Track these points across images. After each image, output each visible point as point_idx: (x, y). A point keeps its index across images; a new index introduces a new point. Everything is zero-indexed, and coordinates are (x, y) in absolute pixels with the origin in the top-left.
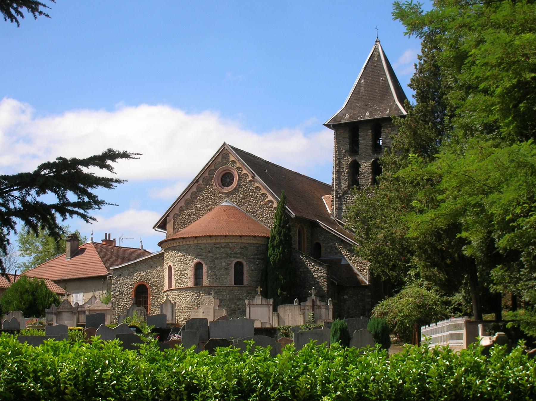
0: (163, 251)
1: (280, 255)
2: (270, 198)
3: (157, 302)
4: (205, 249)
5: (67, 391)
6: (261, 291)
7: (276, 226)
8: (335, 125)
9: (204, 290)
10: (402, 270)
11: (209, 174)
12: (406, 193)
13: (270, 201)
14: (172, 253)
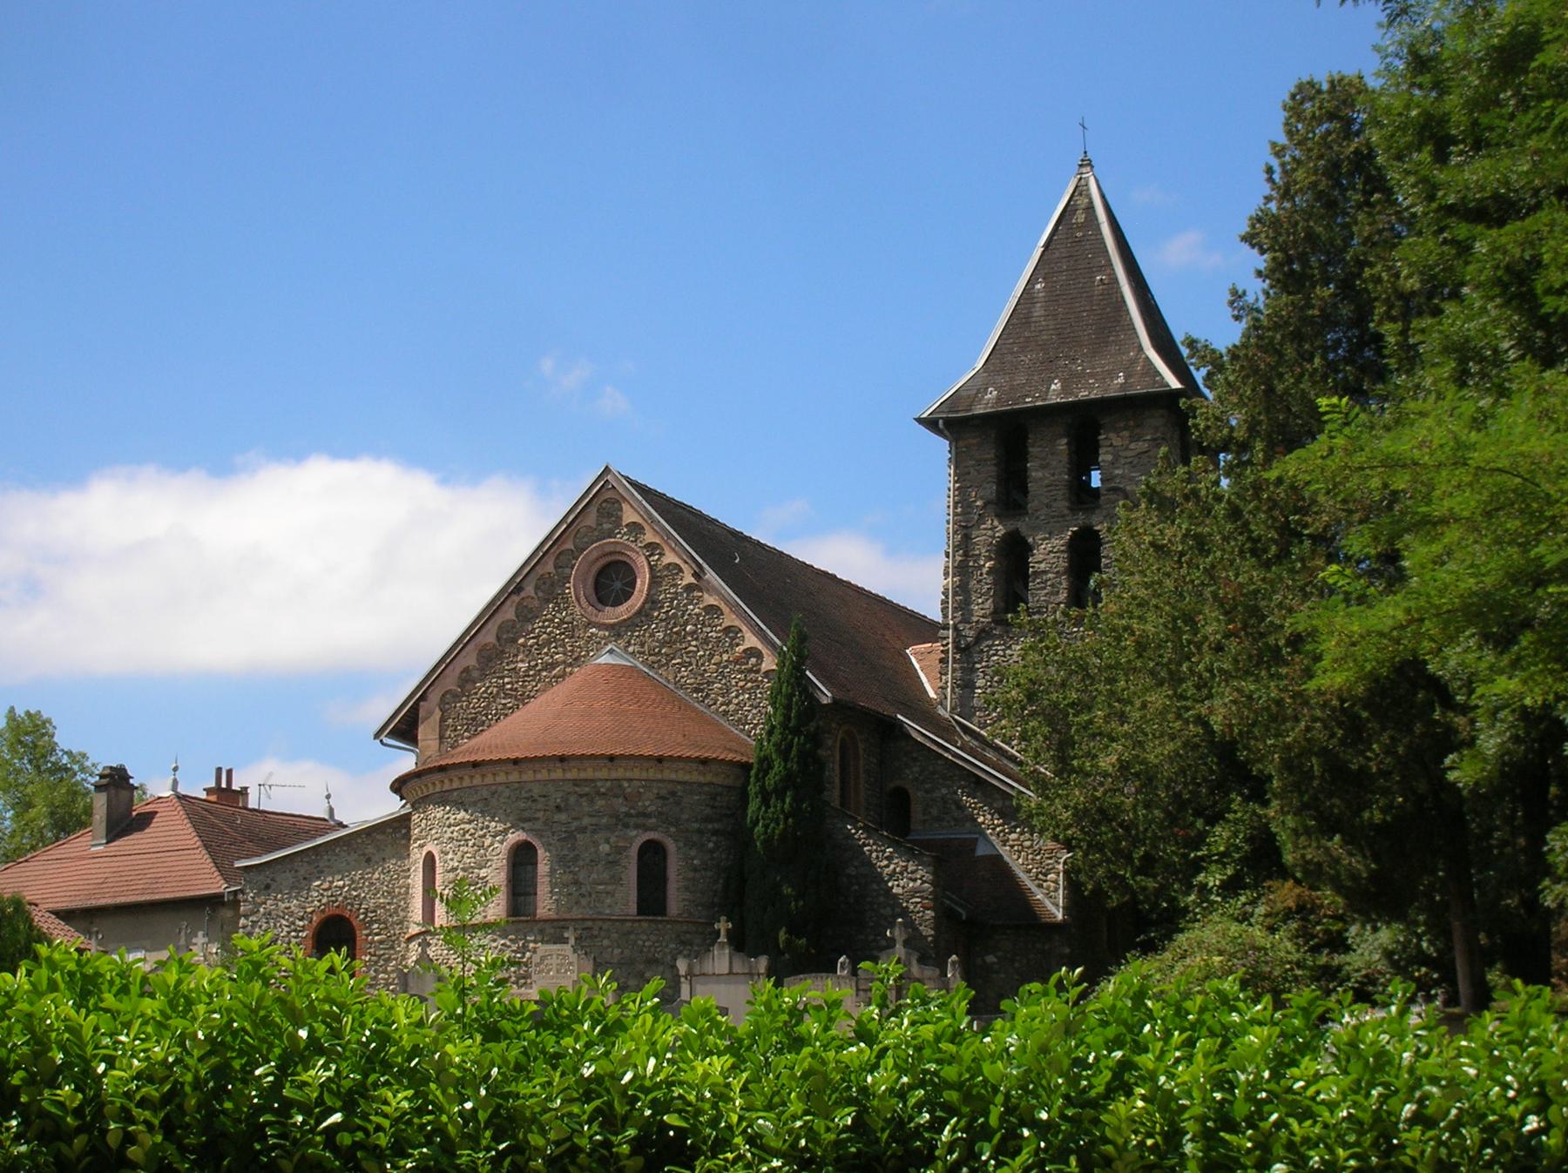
0: (408, 809)
1: (786, 819)
2: (751, 641)
3: (385, 972)
4: (548, 801)
5: (133, 1152)
6: (728, 931)
7: (773, 727)
8: (952, 423)
9: (541, 931)
10: (1176, 873)
12: (1241, 585)
13: (752, 652)
14: (438, 813)
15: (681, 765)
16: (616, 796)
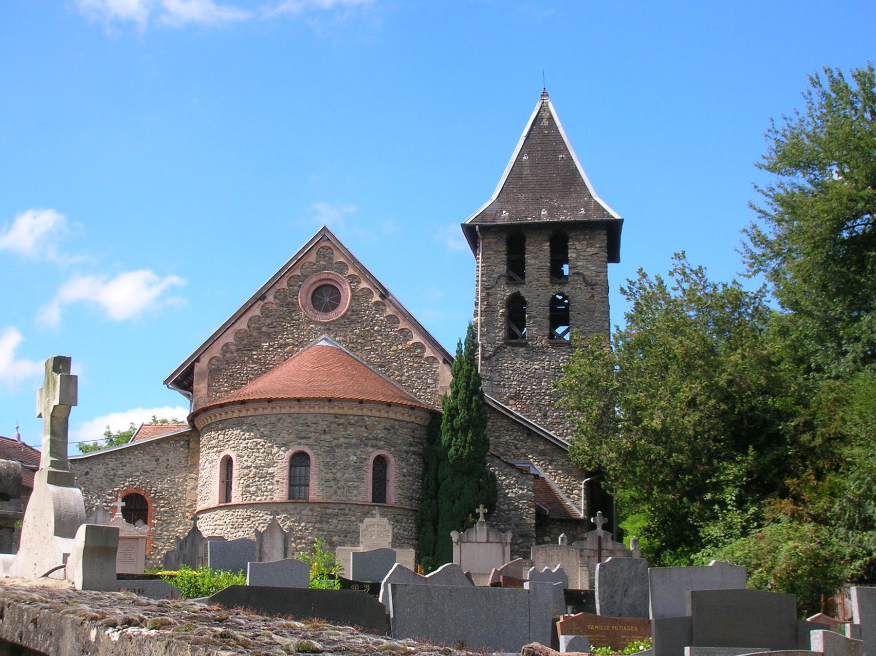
8: (474, 233)
9: (312, 510)
11: (289, 285)
13: (417, 345)
15: (400, 409)
16: (361, 426)
